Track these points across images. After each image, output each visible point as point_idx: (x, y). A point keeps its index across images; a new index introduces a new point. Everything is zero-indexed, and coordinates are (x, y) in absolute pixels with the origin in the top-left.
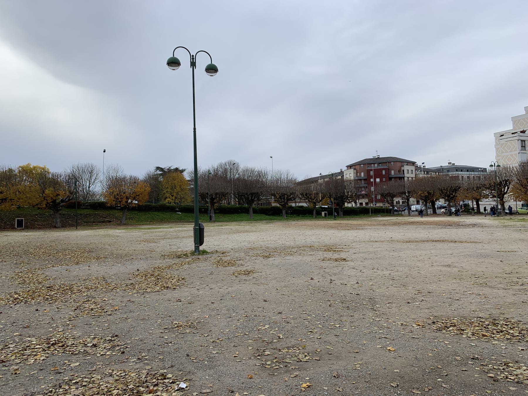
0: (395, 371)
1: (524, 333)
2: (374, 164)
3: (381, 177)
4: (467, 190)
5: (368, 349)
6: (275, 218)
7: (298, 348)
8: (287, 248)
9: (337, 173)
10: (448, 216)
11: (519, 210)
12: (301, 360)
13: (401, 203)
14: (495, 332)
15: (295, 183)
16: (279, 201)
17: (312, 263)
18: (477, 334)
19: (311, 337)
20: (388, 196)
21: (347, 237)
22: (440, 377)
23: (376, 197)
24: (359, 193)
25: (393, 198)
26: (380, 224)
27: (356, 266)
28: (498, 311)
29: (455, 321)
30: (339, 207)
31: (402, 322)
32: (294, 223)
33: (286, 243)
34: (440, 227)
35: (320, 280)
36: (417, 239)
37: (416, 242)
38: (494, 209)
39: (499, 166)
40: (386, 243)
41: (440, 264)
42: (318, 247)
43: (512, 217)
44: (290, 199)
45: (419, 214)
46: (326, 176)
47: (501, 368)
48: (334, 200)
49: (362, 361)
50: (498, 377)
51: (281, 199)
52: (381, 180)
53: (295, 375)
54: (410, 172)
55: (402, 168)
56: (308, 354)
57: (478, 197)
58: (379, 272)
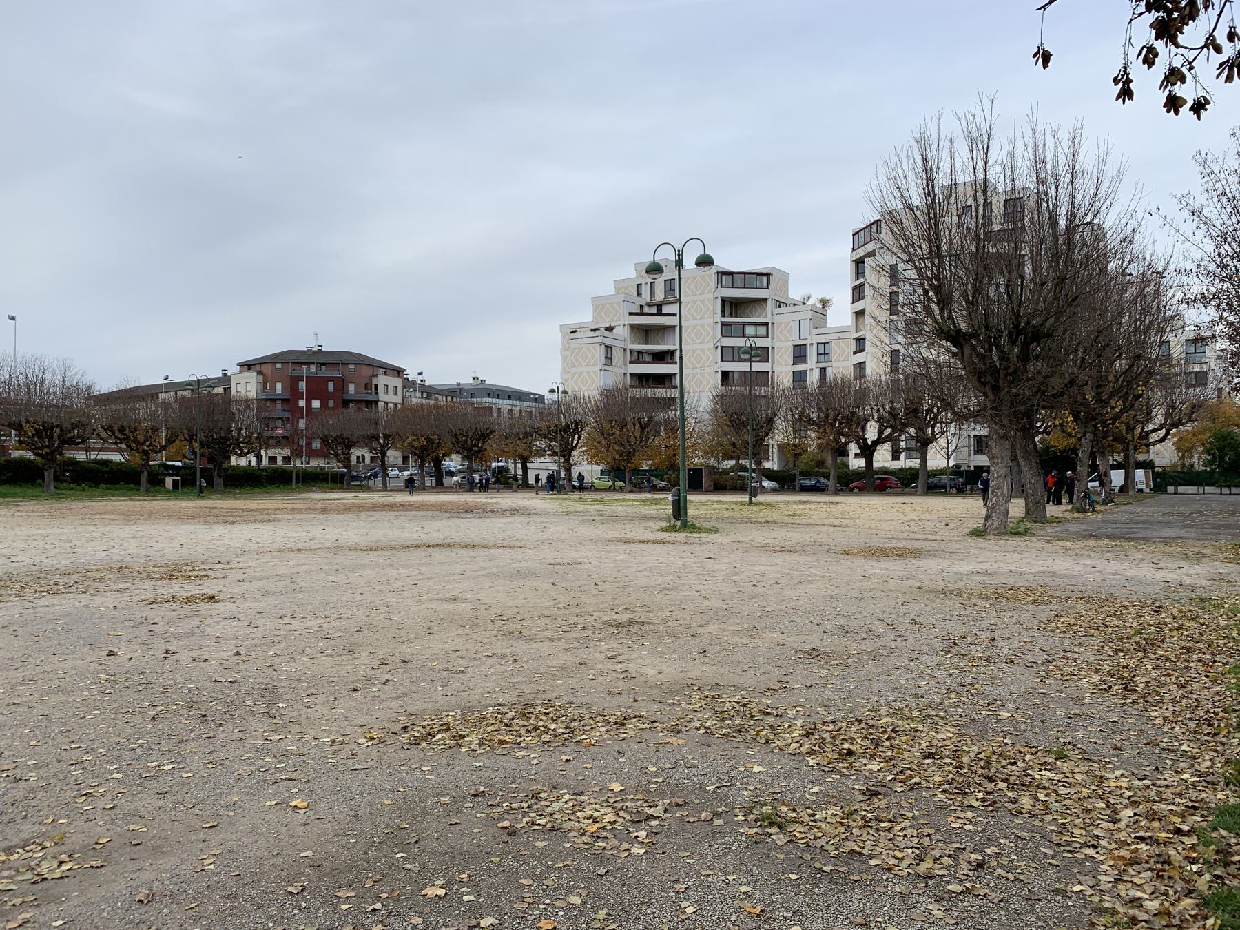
0: (302, 855)
1: (575, 726)
2: (308, 364)
3: (324, 397)
4: (507, 438)
5: (242, 815)
6: (18, 490)
7: (40, 845)
8: (47, 574)
9: (214, 379)
10: (467, 491)
11: (596, 482)
12: (45, 876)
13: (367, 460)
14: (523, 731)
15: (90, 398)
16: (33, 444)
17: (118, 613)
18: (490, 741)
19: (85, 808)
20: (337, 444)
21: (226, 542)
22: (403, 848)
23: (309, 444)
24: (269, 434)
25: (349, 448)
26: (314, 510)
27: (239, 613)
28: (535, 687)
29: (450, 719)
30: (215, 466)
31: (333, 738)
32: (77, 505)
33: (47, 560)
34: (447, 515)
35: (136, 654)
36: (394, 543)
37: (392, 548)
38: (554, 479)
39: (565, 392)
40: (323, 554)
41: (436, 597)
42: (142, 569)
43: (584, 495)
44: (71, 441)
45: (407, 487)
46: (177, 386)
47: (525, 805)
48: (200, 449)
49: (223, 847)
50: (516, 826)
51: (40, 437)
52: (324, 405)
53: (21, 922)
54: (391, 389)
55: (374, 381)
56: (69, 856)
57: (526, 454)
58: (295, 624)
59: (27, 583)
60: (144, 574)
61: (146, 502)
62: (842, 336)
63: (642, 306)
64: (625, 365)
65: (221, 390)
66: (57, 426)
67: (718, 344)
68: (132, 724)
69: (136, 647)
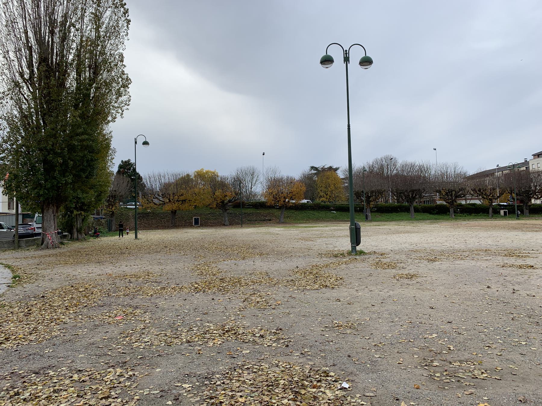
6: (441, 217)
8: (457, 251)
9: (520, 164)
16: (445, 198)
19: (489, 352)
21: (535, 240)
30: (524, 204)
32: (464, 223)
33: (456, 245)
42: (495, 251)
44: (460, 196)
51: (448, 195)
56: (485, 371)
59: (450, 254)
60: (497, 253)
61: (492, 221)
65: (524, 168)
66: (454, 190)
68: (503, 320)
69: (499, 286)
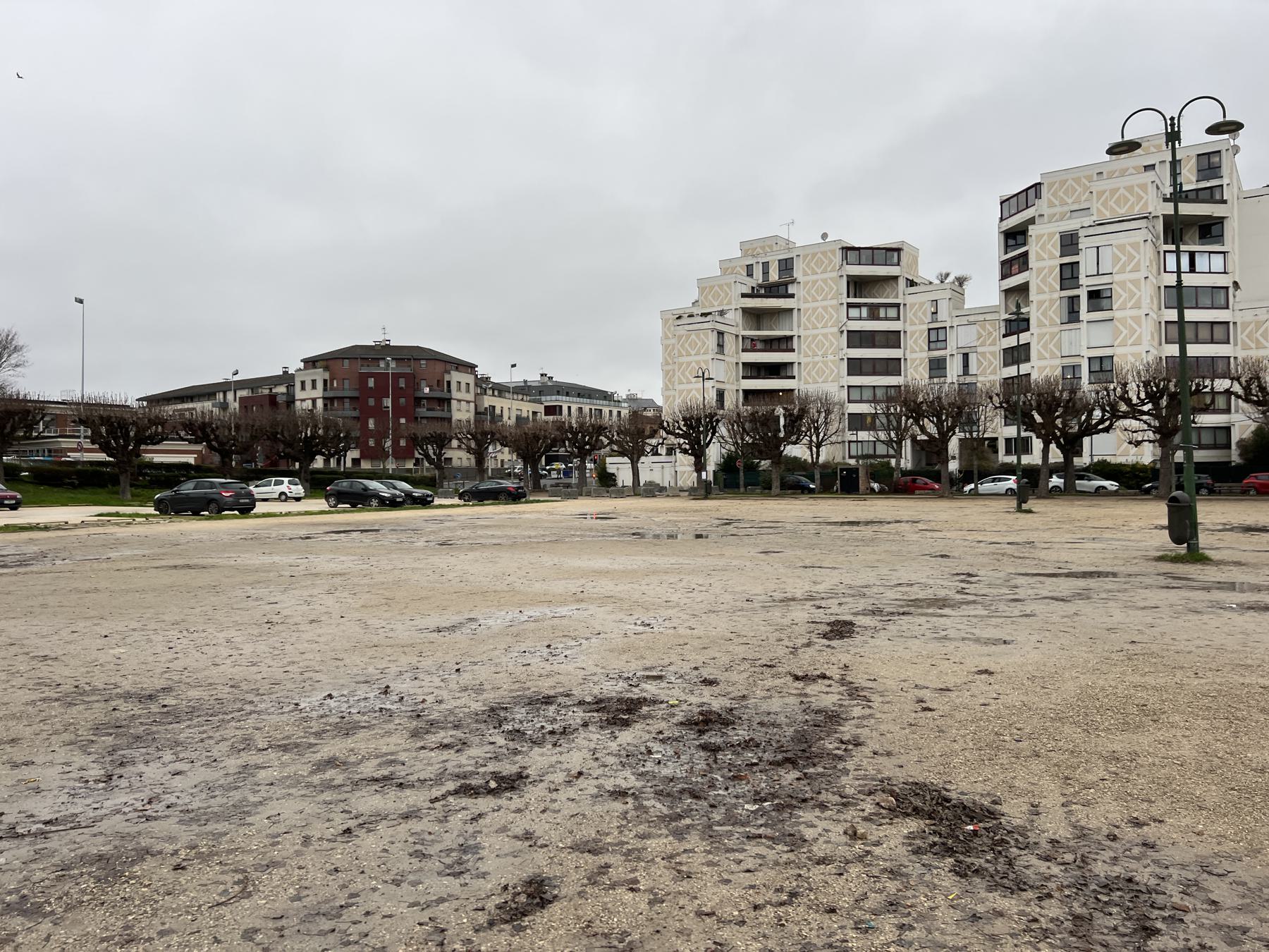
54: (463, 386)
55: (447, 378)
62: (988, 317)
63: (753, 288)
64: (737, 353)
67: (844, 328)
